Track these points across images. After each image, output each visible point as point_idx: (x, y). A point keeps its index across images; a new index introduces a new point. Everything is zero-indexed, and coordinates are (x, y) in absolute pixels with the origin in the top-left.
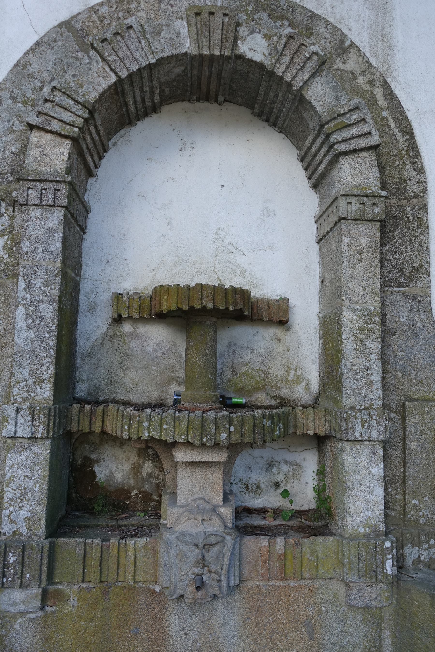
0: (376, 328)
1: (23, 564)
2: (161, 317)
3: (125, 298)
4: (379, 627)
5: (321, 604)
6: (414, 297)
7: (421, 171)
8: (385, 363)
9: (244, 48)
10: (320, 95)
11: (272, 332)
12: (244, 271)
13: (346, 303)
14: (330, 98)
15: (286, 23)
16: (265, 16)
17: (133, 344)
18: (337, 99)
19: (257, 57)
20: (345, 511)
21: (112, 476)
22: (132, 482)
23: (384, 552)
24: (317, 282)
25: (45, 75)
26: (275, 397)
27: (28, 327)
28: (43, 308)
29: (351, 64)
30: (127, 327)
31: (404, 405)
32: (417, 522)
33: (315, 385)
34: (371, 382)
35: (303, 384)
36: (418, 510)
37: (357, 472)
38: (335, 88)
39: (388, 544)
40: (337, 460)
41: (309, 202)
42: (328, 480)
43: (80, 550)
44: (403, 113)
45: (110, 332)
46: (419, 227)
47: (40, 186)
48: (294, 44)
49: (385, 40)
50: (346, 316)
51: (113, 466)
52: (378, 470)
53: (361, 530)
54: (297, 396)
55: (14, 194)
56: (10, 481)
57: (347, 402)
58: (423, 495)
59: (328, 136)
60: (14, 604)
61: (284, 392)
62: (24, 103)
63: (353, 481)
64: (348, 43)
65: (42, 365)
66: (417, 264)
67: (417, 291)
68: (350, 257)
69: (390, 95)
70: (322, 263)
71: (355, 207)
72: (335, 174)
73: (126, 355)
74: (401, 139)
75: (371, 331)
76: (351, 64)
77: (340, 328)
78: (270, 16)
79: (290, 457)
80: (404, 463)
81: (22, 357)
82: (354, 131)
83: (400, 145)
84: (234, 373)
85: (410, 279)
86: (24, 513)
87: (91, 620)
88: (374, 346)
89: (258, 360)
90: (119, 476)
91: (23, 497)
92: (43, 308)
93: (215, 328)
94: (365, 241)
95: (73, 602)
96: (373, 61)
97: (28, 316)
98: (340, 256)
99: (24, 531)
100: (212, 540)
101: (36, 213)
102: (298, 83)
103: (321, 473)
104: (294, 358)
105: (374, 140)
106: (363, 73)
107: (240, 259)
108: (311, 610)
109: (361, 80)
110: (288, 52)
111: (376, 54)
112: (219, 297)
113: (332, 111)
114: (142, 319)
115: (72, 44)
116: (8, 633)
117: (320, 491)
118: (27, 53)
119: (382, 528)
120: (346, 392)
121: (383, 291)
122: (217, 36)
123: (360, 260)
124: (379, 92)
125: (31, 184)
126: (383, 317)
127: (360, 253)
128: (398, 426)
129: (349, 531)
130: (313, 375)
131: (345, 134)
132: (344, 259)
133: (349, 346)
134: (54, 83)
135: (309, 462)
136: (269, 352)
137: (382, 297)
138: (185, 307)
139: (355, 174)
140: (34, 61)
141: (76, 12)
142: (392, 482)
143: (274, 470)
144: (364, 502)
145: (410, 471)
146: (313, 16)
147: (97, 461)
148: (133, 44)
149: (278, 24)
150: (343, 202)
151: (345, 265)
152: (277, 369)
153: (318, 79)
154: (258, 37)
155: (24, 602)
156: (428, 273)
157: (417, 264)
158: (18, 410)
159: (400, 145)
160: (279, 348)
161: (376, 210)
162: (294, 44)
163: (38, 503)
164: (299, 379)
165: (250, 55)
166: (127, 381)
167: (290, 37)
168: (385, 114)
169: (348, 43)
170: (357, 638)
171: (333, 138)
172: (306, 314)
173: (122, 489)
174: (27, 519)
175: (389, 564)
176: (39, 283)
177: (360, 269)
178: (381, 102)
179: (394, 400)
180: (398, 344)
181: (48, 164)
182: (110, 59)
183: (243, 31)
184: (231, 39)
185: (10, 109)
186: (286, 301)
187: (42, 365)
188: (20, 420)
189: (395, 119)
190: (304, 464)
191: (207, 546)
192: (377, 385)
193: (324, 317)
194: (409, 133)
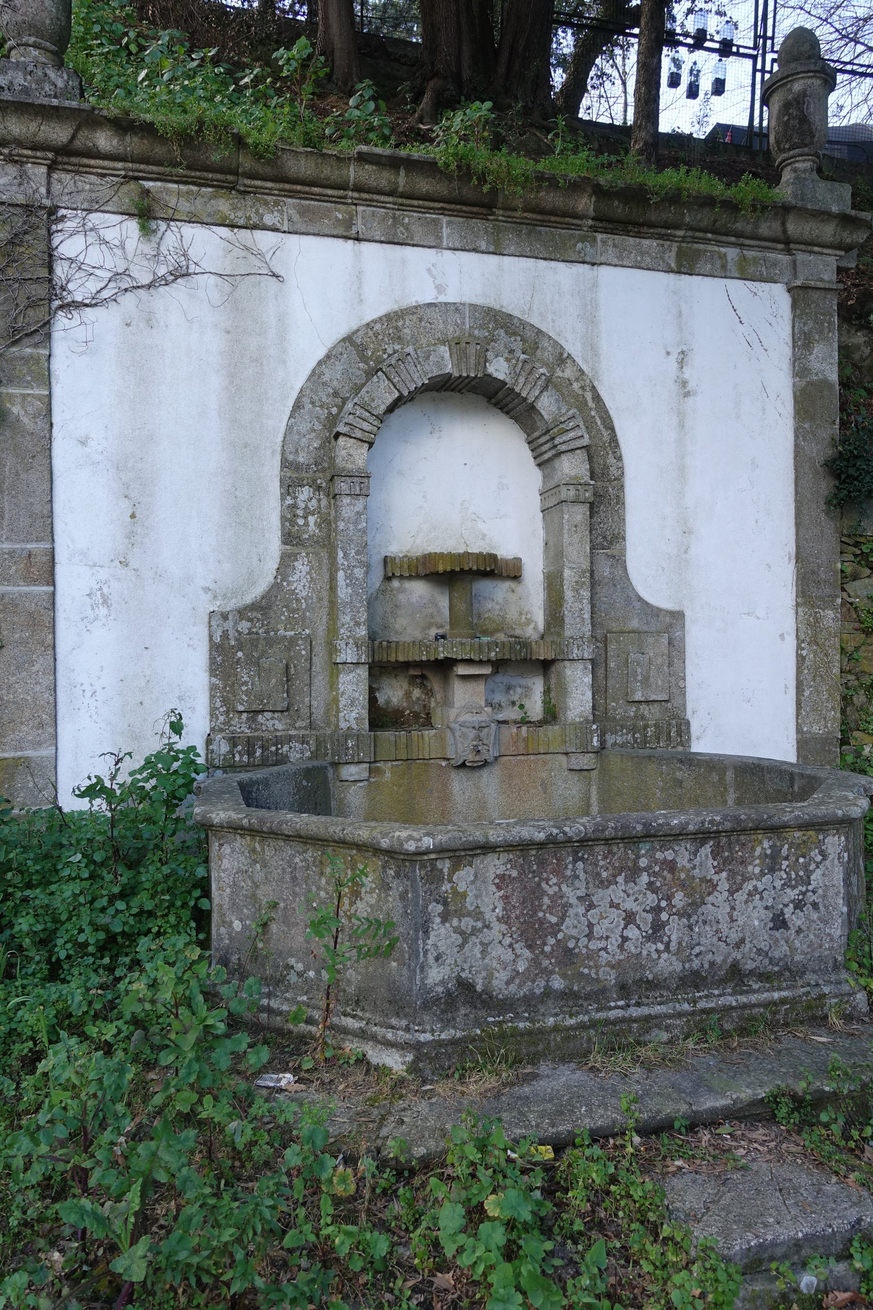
0: (587, 581)
1: (358, 746)
2: (418, 577)
3: (397, 560)
4: (589, 784)
5: (551, 770)
6: (614, 557)
7: (619, 458)
8: (593, 606)
9: (491, 369)
10: (547, 405)
11: (508, 584)
12: (484, 536)
13: (567, 563)
14: (554, 408)
15: (519, 338)
16: (502, 332)
17: (401, 597)
18: (559, 409)
19: (501, 376)
20: (566, 708)
21: (388, 702)
22: (405, 704)
23: (592, 732)
24: (542, 544)
25: (335, 383)
26: (511, 636)
27: (347, 585)
28: (356, 571)
29: (568, 373)
30: (396, 583)
31: (606, 637)
32: (614, 718)
33: (541, 626)
34: (583, 619)
35: (532, 626)
36: (615, 710)
37: (574, 681)
38: (557, 400)
39: (594, 727)
40: (560, 676)
41: (535, 477)
42: (553, 694)
43: (392, 738)
44: (607, 412)
45: (383, 588)
46: (617, 503)
47: (349, 480)
48: (528, 367)
49: (593, 349)
50: (567, 573)
51: (390, 693)
52: (588, 679)
53: (577, 720)
54: (528, 635)
55: (319, 481)
56: (343, 693)
57: (567, 633)
58: (619, 699)
59: (553, 439)
60: (352, 775)
61: (518, 632)
62: (321, 407)
63: (571, 687)
64: (565, 355)
65: (359, 612)
66: (616, 532)
67: (615, 553)
68: (569, 530)
69: (597, 398)
70: (546, 528)
71: (572, 493)
72: (557, 463)
73: (396, 606)
74: (605, 433)
75: (584, 583)
76: (568, 373)
77: (562, 581)
78: (506, 333)
79: (523, 682)
80: (606, 677)
81: (344, 607)
82: (571, 435)
83: (605, 439)
84: (479, 617)
85: (611, 543)
86: (354, 715)
87: (400, 786)
88: (586, 593)
89: (498, 607)
90: (395, 700)
91: (352, 704)
92: (356, 571)
93: (471, 582)
94: (579, 518)
95: (388, 775)
96: (584, 368)
97: (347, 577)
98: (562, 529)
99: (355, 727)
100: (484, 724)
101: (347, 500)
102: (531, 399)
103: (547, 691)
104: (525, 605)
105: (586, 441)
106: (577, 380)
107: (480, 525)
108: (544, 775)
109: (576, 386)
110: (524, 374)
111: (586, 361)
112: (480, 562)
113: (555, 419)
114: (410, 578)
115: (355, 356)
116: (345, 797)
117: (546, 703)
118: (320, 363)
119: (591, 718)
120: (567, 626)
121: (591, 553)
122: (472, 361)
123: (576, 532)
124: (589, 396)
125: (343, 479)
126: (592, 572)
127: (576, 526)
128: (602, 651)
129: (569, 720)
130: (539, 618)
131: (565, 438)
132: (565, 531)
133: (569, 594)
134: (356, 400)
135: (537, 685)
136: (506, 601)
137: (591, 557)
138: (458, 569)
139: (573, 467)
140: (326, 371)
141: (355, 328)
142: (598, 690)
143: (512, 692)
144: (579, 701)
145: (611, 682)
146: (539, 332)
147: (378, 689)
148: (412, 368)
149: (512, 339)
150: (564, 489)
151: (566, 536)
152: (512, 615)
153: (545, 393)
154: (501, 359)
155: (358, 773)
156: (624, 539)
157: (616, 532)
158: (347, 644)
159: (605, 439)
160: (513, 598)
161: (587, 495)
162: (528, 367)
163: (363, 708)
164: (529, 622)
165: (495, 375)
166: (397, 626)
167: (525, 361)
168: (593, 413)
169: (565, 355)
170: (574, 792)
171: (557, 441)
172: (534, 571)
173: (398, 710)
174: (356, 718)
175: (595, 739)
176: (353, 553)
177: (576, 538)
178: (591, 404)
179: (599, 632)
180: (603, 592)
181: (353, 463)
182: (395, 381)
183: (490, 355)
184: (482, 363)
185: (310, 412)
186: (519, 560)
187: (359, 612)
188: (349, 651)
189: (601, 417)
190: (534, 687)
191: (481, 728)
192: (588, 621)
193: (548, 572)
194: (612, 429)
